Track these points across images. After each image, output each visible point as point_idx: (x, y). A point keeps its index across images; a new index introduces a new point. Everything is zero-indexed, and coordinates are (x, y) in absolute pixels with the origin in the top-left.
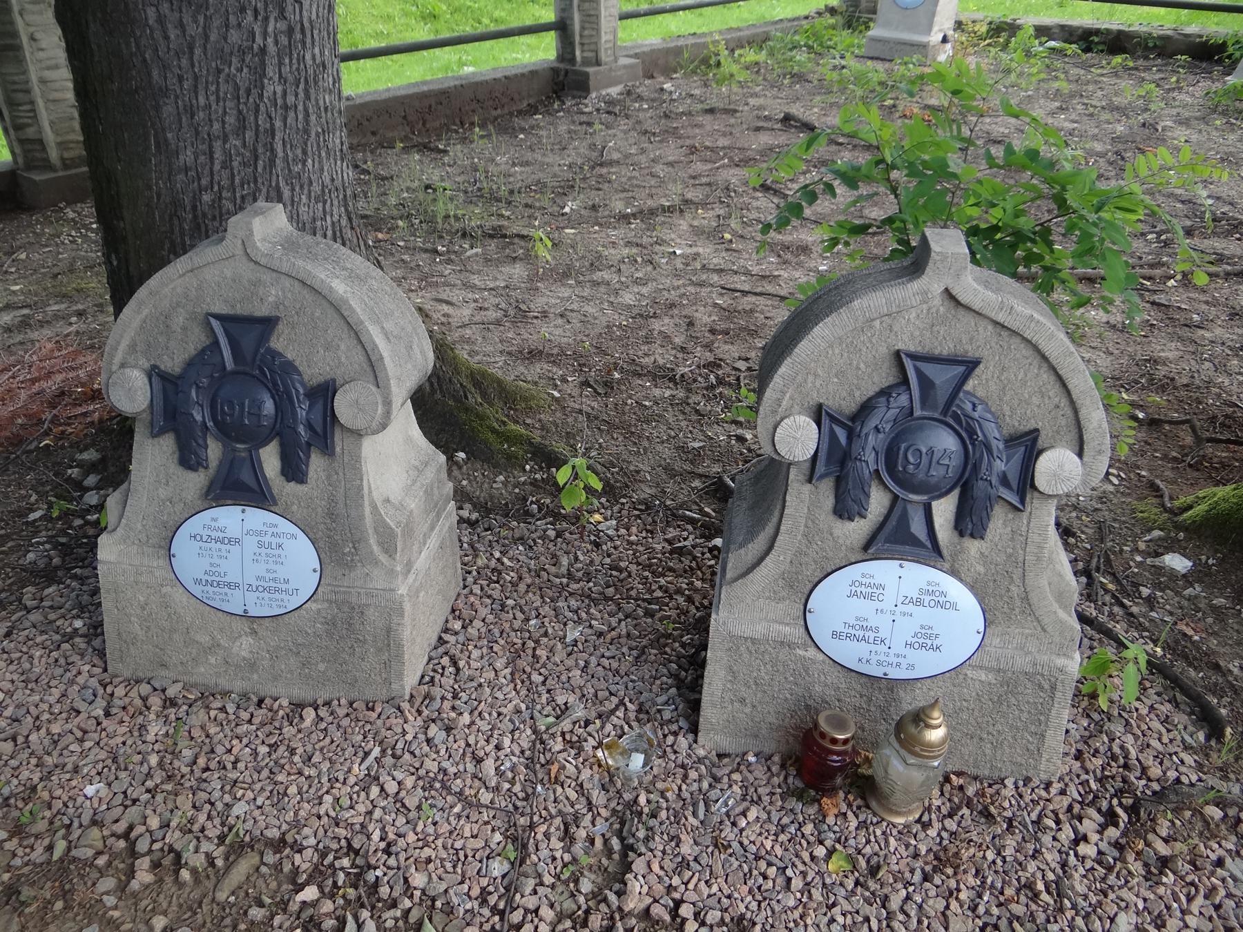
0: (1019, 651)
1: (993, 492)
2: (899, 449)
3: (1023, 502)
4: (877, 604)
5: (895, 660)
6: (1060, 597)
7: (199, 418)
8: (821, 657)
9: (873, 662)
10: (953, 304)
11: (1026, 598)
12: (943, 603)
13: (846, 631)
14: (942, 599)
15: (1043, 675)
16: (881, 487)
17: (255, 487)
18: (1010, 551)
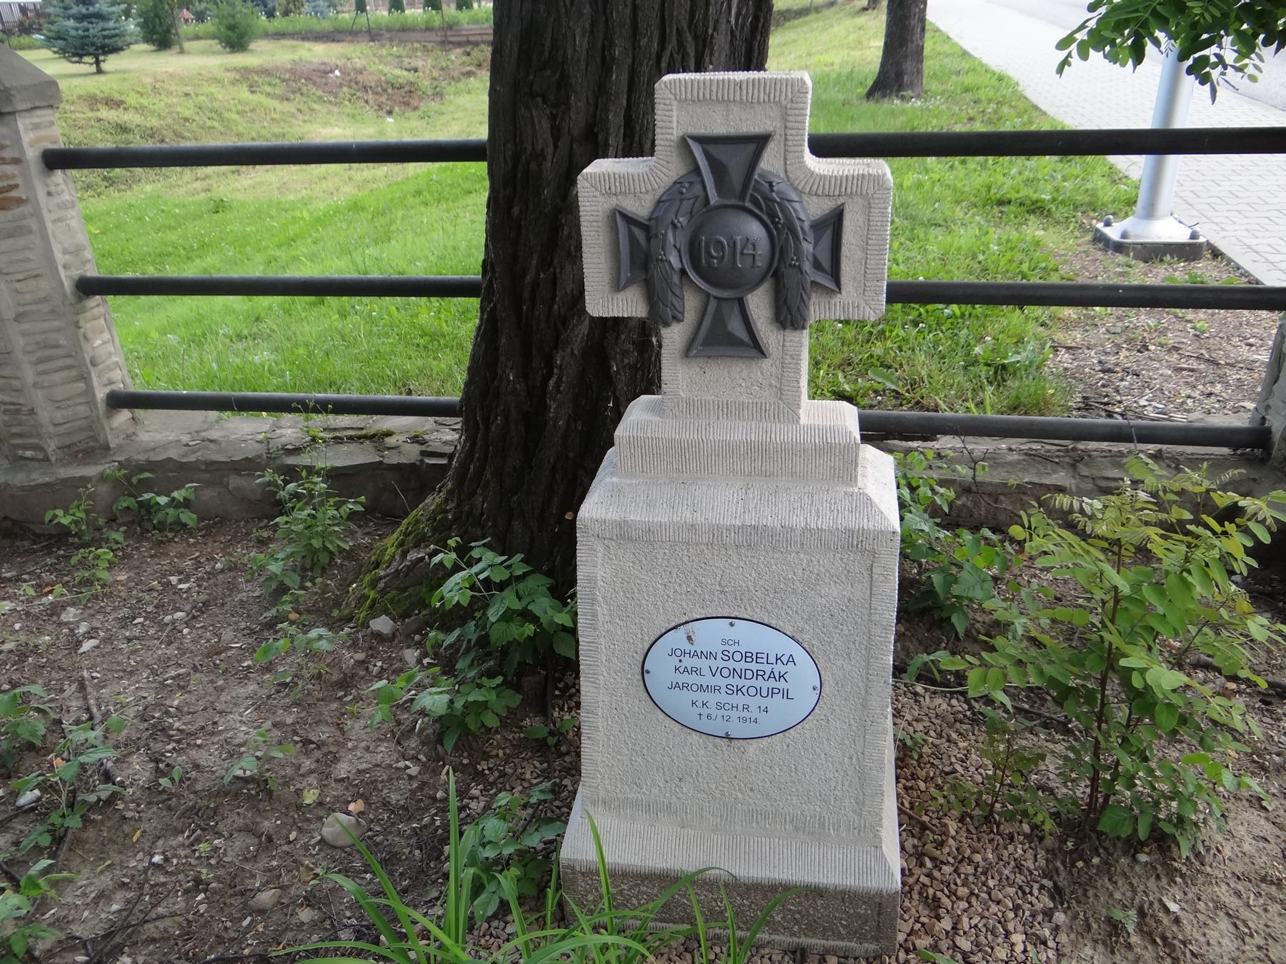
2: (700, 244)
7: (676, 264)
17: (741, 334)
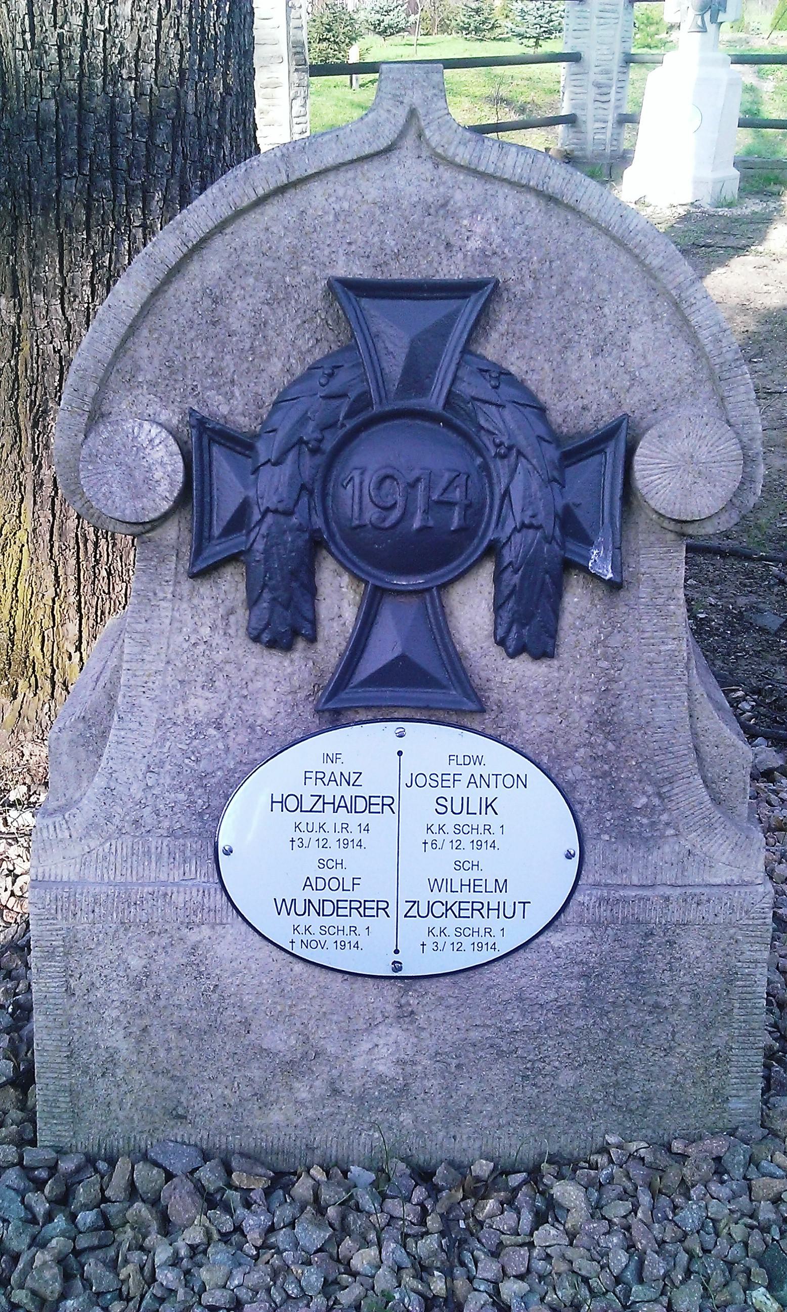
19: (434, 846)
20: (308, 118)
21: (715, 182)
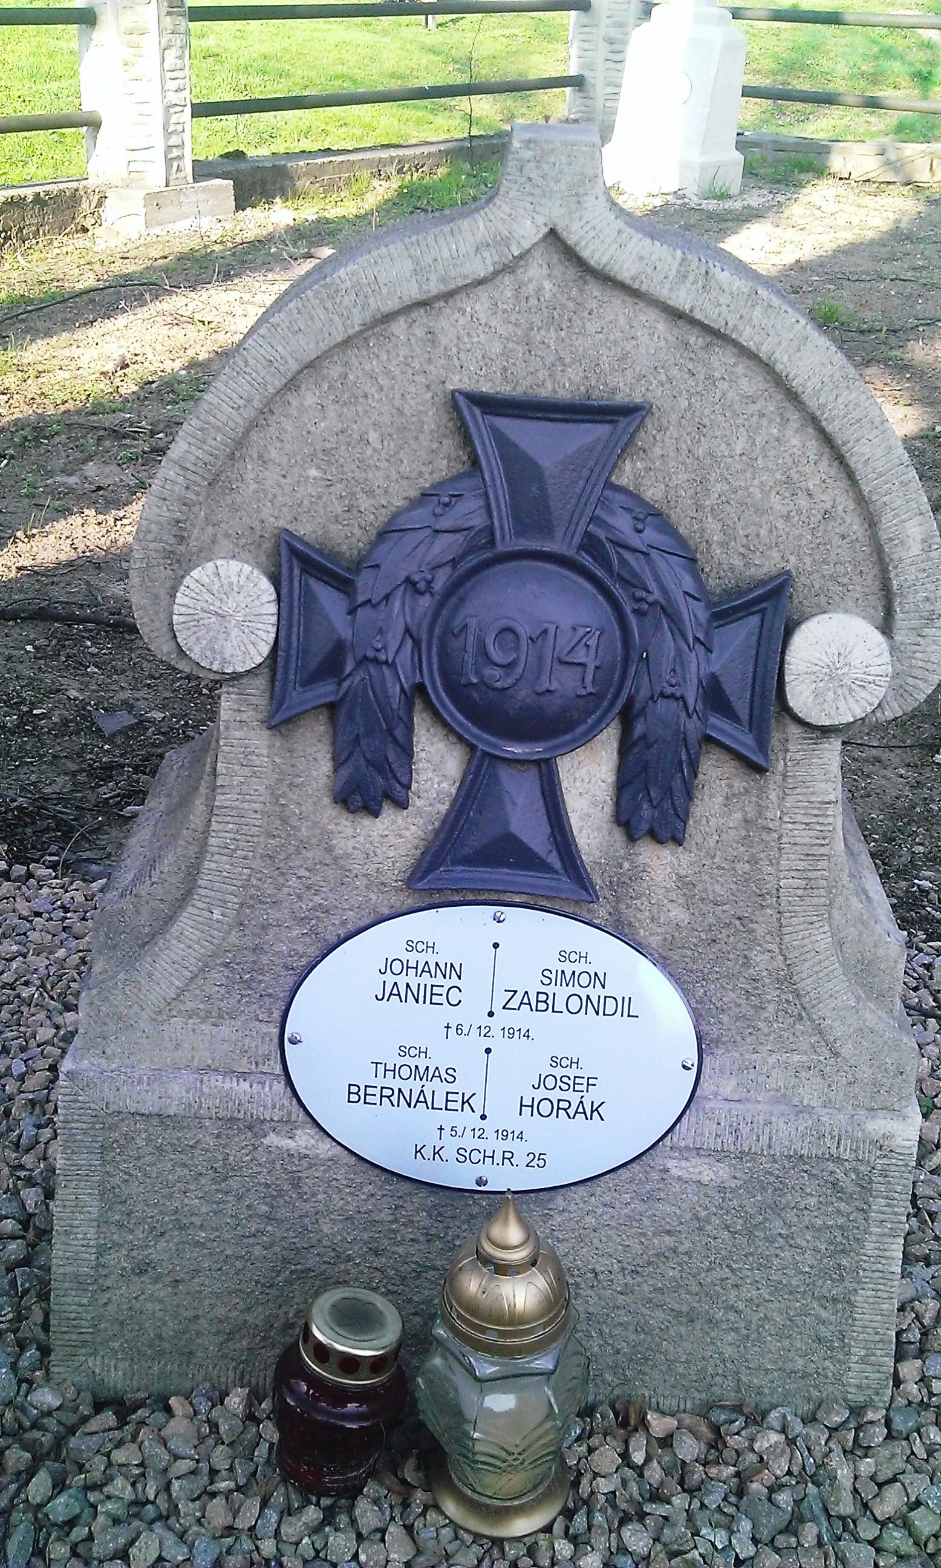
0: (781, 1104)
1: (692, 726)
3: (762, 745)
4: (453, 1016)
5: (500, 1146)
6: (863, 971)
8: (325, 1148)
9: (449, 1153)
10: (572, 273)
11: (787, 980)
12: (601, 1003)
13: (380, 1082)
14: (595, 992)
15: (838, 1160)
16: (440, 731)
18: (743, 867)
19: (459, 1032)
20: (187, 71)
21: (704, 168)
